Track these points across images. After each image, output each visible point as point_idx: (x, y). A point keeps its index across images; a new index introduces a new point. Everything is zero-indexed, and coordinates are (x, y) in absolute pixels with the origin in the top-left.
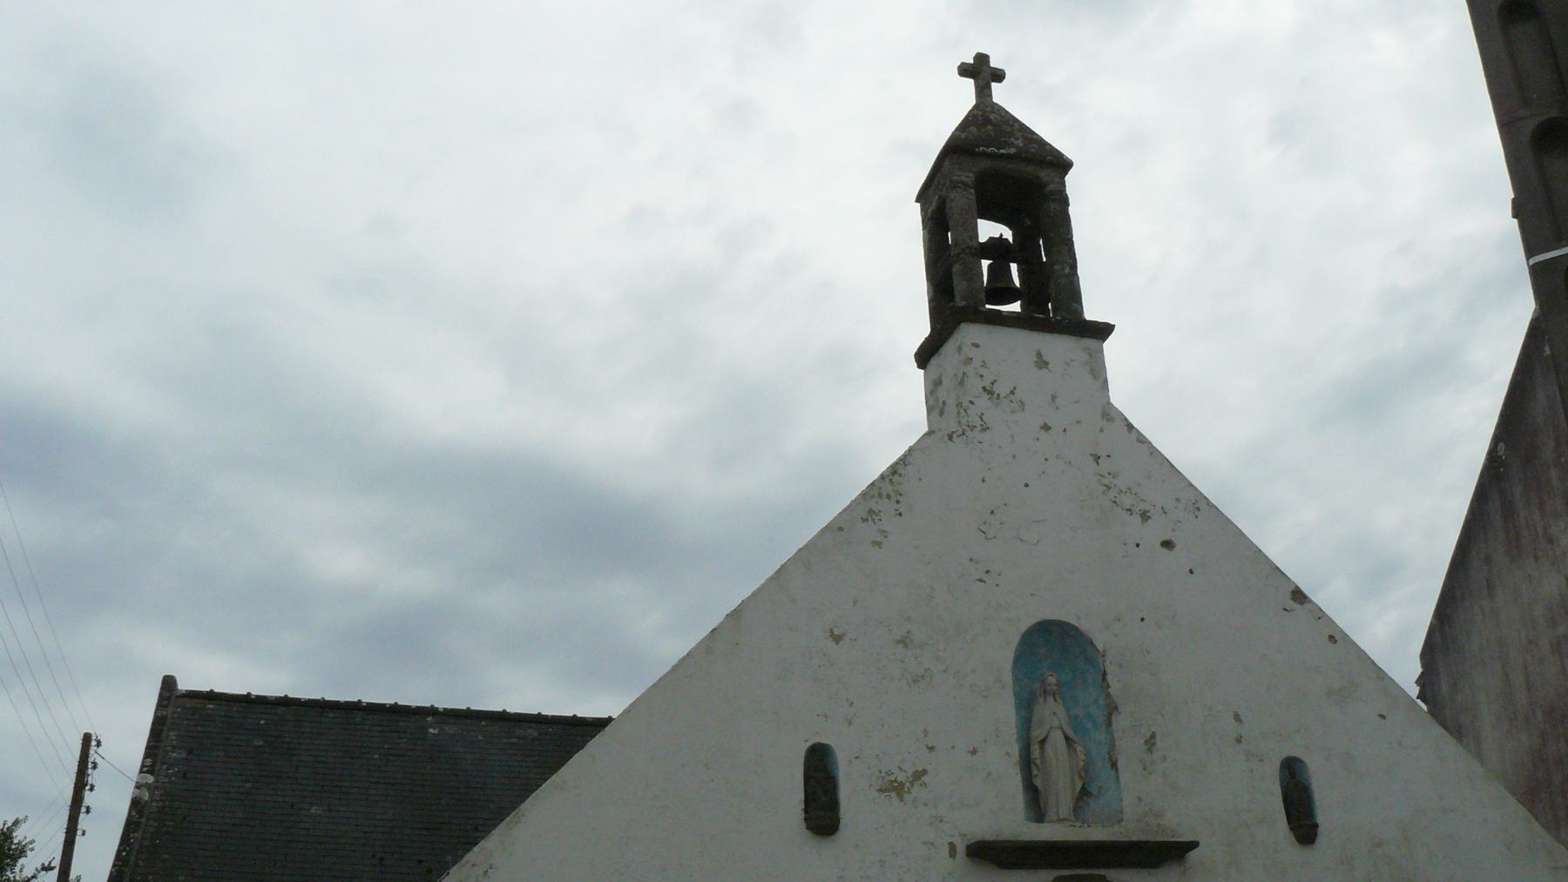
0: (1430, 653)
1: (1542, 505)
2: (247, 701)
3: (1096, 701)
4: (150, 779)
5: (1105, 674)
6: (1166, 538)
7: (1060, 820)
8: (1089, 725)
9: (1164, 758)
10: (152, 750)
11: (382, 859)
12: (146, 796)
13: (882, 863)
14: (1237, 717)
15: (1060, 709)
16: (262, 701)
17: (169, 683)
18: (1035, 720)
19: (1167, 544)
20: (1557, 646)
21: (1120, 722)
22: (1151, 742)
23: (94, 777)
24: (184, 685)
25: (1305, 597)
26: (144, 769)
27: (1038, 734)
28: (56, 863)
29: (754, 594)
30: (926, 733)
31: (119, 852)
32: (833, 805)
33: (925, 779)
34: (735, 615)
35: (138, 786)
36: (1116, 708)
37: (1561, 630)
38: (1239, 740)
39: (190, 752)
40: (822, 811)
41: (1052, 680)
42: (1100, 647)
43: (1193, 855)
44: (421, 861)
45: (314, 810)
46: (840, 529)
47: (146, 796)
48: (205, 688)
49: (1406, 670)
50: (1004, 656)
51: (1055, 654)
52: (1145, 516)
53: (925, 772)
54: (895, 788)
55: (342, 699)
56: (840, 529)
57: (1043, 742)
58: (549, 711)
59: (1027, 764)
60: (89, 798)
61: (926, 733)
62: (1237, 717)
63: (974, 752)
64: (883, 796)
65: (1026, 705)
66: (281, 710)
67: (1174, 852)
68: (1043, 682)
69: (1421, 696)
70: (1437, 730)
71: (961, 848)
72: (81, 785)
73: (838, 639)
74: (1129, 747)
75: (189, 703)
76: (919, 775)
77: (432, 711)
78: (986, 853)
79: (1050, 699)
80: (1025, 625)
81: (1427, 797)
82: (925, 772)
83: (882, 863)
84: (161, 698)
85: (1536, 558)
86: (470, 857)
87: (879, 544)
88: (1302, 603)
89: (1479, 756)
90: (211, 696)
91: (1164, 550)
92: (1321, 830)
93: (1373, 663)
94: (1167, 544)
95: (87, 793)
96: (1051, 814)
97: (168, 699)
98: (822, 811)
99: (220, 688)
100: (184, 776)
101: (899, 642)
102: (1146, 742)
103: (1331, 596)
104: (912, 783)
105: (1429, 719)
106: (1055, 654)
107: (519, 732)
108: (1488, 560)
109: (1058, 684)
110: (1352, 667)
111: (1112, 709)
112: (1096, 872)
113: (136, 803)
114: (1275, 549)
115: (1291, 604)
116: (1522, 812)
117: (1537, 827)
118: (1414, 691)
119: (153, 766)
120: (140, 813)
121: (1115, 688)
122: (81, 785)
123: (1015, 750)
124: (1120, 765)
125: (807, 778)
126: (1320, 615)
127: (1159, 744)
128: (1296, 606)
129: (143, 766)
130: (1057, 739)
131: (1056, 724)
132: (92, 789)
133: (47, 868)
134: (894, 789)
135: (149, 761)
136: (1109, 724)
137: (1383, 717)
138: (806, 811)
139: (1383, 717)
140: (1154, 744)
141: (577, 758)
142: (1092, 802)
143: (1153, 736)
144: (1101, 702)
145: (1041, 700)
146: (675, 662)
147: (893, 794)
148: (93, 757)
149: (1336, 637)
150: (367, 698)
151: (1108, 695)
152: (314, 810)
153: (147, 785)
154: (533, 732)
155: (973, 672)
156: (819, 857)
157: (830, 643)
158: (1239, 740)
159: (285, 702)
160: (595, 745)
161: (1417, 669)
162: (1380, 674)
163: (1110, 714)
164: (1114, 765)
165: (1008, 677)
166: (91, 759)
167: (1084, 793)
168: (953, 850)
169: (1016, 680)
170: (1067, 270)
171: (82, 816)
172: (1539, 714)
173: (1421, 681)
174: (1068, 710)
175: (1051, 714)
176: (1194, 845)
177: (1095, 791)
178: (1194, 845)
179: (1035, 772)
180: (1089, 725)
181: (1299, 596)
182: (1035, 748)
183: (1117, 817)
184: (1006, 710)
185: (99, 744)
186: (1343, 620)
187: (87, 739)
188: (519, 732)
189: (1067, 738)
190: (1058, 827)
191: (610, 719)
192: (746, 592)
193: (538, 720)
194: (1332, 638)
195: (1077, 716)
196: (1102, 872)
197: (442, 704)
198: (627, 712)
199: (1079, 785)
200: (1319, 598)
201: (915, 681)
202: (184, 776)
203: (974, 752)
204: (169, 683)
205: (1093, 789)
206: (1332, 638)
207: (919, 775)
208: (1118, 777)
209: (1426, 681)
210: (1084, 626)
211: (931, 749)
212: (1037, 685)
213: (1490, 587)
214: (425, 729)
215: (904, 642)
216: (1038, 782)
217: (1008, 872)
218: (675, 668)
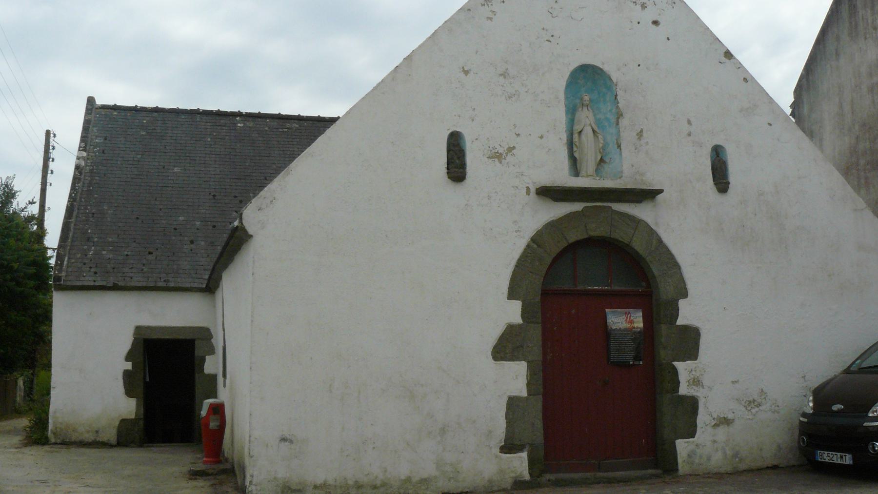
0: (799, 91)
1: (873, 8)
2: (135, 110)
4: (85, 154)
5: (616, 96)
6: (655, 19)
7: (588, 176)
9: (647, 143)
10: (84, 138)
11: (214, 196)
12: (83, 163)
13: (489, 197)
14: (689, 122)
15: (590, 114)
16: (143, 110)
17: (91, 101)
19: (655, 23)
20: (871, 90)
21: (624, 122)
22: (640, 134)
23: (53, 154)
24: (99, 102)
25: (732, 55)
26: (80, 149)
27: (577, 128)
28: (37, 199)
29: (420, 47)
31: (70, 194)
32: (463, 166)
33: (514, 151)
34: (409, 59)
35: (78, 158)
36: (622, 115)
37: (875, 79)
38: (689, 135)
39: (105, 139)
40: (456, 169)
41: (587, 98)
42: (614, 80)
44: (235, 197)
45: (176, 170)
46: (469, 10)
47: (83, 163)
48: (111, 103)
49: (785, 99)
50: (560, 83)
51: (588, 81)
52: (644, 6)
53: (514, 148)
54: (497, 156)
55: (189, 107)
56: (469, 10)
57: (580, 132)
58: (305, 113)
59: (571, 144)
60: (52, 166)
62: (689, 122)
63: (541, 137)
65: (572, 112)
66: (155, 114)
68: (582, 99)
69: (793, 114)
70: (800, 133)
71: (533, 190)
72: (47, 159)
73: (466, 73)
74: (628, 136)
75: (103, 112)
76: (511, 149)
77: (239, 114)
79: (585, 109)
80: (572, 68)
81: (797, 175)
82: (514, 148)
83: (489, 197)
84: (87, 109)
85: (866, 38)
86: (262, 193)
87: (491, 19)
89: (821, 148)
90: (115, 108)
91: (654, 26)
92: (730, 186)
93: (767, 94)
94: (655, 23)
95: (51, 163)
96: (583, 173)
97: (91, 110)
98: (456, 169)
99: (121, 103)
100: (103, 152)
101: (501, 75)
102: (637, 134)
103: (750, 58)
104: (507, 154)
105: (796, 126)
106: (588, 81)
107: (288, 125)
108: (838, 39)
109: (591, 100)
110: (760, 98)
111: (619, 115)
112: (605, 204)
113: (77, 167)
114: (717, 29)
115: (724, 59)
116: (842, 179)
117: (849, 188)
118: (789, 111)
119: (85, 147)
120: (80, 173)
122: (47, 159)
123: (564, 137)
125: (449, 151)
126: (740, 66)
127: (645, 135)
128: (727, 61)
129: (80, 147)
130: (588, 131)
131: (588, 122)
132: (53, 160)
133: (32, 203)
135: (83, 145)
136: (618, 124)
137: (770, 125)
138: (448, 168)
139: (770, 125)
140: (641, 136)
141: (320, 139)
142: (606, 166)
143: (642, 131)
146: (375, 85)
147: (496, 160)
148: (52, 143)
149: (747, 79)
150: (203, 107)
152: (176, 170)
153: (83, 158)
154: (295, 125)
155: (543, 92)
156: (453, 193)
157: (462, 75)
159: (157, 110)
160: (330, 132)
161: (791, 99)
162: (771, 101)
163: (618, 118)
164: (619, 146)
165: (562, 96)
166: (51, 144)
167: (602, 160)
169: (566, 98)
171: (49, 175)
172: (857, 127)
173: (794, 106)
174: (595, 115)
175: (585, 117)
176: (660, 191)
177: (607, 161)
178: (660, 191)
179: (575, 149)
181: (728, 55)
182: (576, 136)
184: (560, 114)
185: (55, 136)
186: (753, 70)
187: (48, 133)
188: (288, 125)
189: (594, 131)
190: (584, 179)
191: (339, 118)
192: (415, 46)
193: (299, 118)
194: (745, 80)
196: (609, 204)
197: (244, 110)
198: (348, 113)
200: (740, 57)
201: (510, 97)
202: (103, 152)
203: (541, 137)
204: (91, 101)
205: (607, 159)
206: (745, 80)
207: (511, 149)
208: (621, 154)
209: (795, 106)
210: (606, 68)
211: (518, 135)
212: (578, 101)
213: (837, 54)
214: (235, 124)
215: (504, 75)
216: (576, 155)
218: (375, 88)
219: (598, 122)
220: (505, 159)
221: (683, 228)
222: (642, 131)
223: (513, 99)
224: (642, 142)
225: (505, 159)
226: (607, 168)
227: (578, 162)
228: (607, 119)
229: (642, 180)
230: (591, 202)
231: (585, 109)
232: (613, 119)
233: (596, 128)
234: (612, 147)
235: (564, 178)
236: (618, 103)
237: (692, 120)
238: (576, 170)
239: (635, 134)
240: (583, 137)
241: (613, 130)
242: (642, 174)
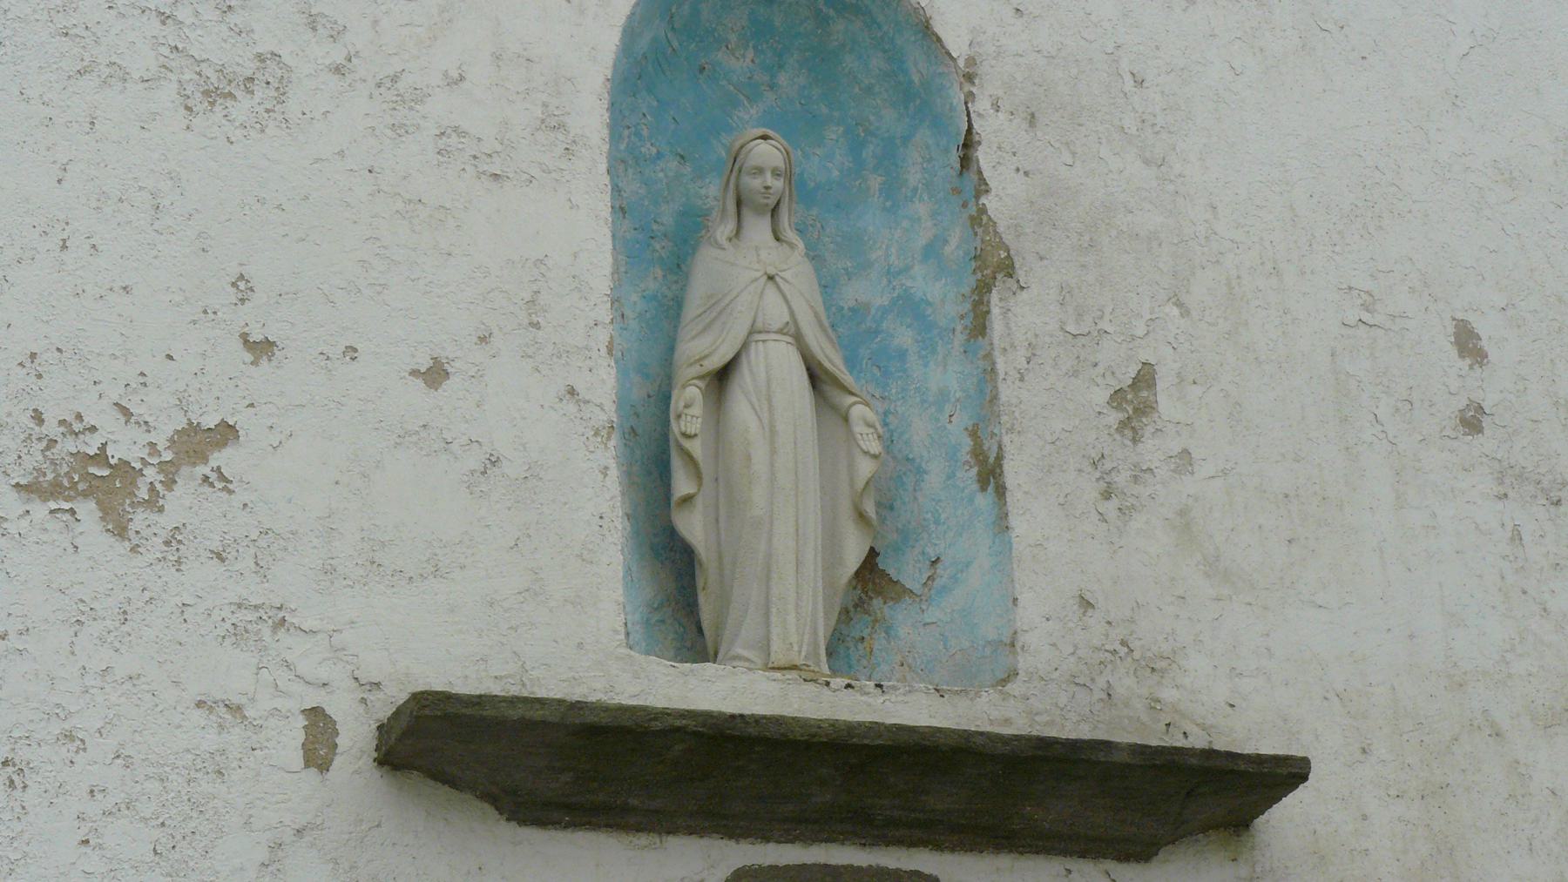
3: (932, 251)
5: (969, 143)
8: (905, 337)
14: (1467, 343)
18: (693, 307)
21: (1021, 316)
22: (1136, 399)
27: (703, 348)
30: (242, 287)
36: (1008, 268)
38: (1472, 421)
41: (767, 153)
42: (956, 43)
43: (1286, 819)
53: (226, 433)
57: (722, 377)
59: (653, 463)
61: (242, 287)
62: (1467, 343)
63: (435, 374)
64: (40, 510)
65: (662, 250)
67: (1231, 790)
71: (356, 735)
74: (1050, 413)
76: (201, 442)
78: (454, 748)
79: (758, 229)
82: (226, 433)
88: (1304, 778)
102: (1117, 398)
111: (993, 268)
121: (1006, 196)
123: (602, 385)
124: (1015, 472)
127: (1167, 404)
130: (776, 371)
131: (775, 313)
134: (94, 489)
136: (979, 325)
140: (1145, 409)
142: (904, 621)
143: (1145, 378)
144: (956, 244)
145: (724, 230)
147: (87, 510)
151: (979, 219)
158: (1472, 421)
163: (983, 288)
164: (991, 474)
165: (591, 116)
167: (871, 577)
168: (320, 735)
170: (1003, 255)
174: (827, 287)
176: (1286, 774)
178: (1286, 774)
179: (682, 485)
180: (905, 337)
182: (690, 398)
183: (1000, 662)
184: (572, 228)
189: (816, 376)
195: (859, 311)
199: (853, 558)
203: (435, 374)
205: (906, 570)
208: (1002, 524)
211: (261, 349)
212: (712, 189)
216: (693, 527)
217: (534, 836)
219: (849, 323)
220: (153, 503)
221: (1471, 317)
222: (1145, 378)
223: (242, 108)
224: (1152, 450)
225: (153, 503)
226: (906, 625)
227: (708, 580)
228: (910, 307)
229: (1154, 704)
230: (789, 838)
231: (758, 229)
232: (944, 296)
233: (831, 358)
234: (943, 485)
235: (585, 648)
236: (982, 187)
237: (1487, 328)
238: (679, 592)
239: (1101, 396)
240: (742, 406)
241: (946, 374)
242: (1154, 668)
